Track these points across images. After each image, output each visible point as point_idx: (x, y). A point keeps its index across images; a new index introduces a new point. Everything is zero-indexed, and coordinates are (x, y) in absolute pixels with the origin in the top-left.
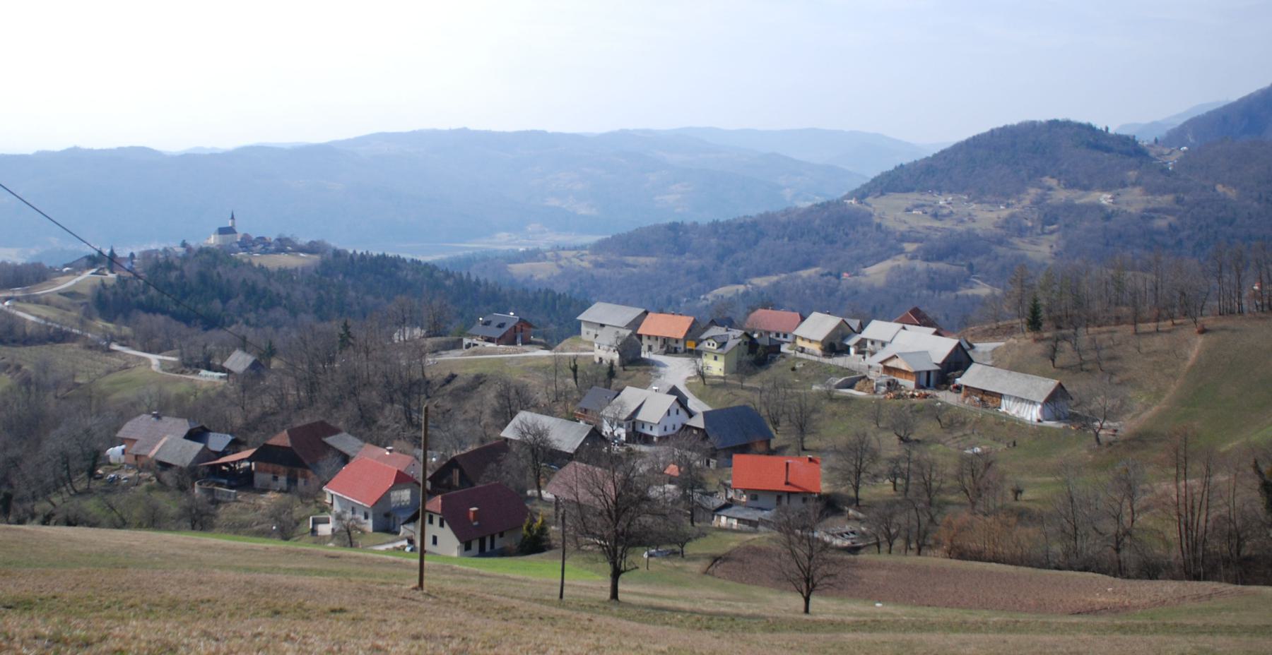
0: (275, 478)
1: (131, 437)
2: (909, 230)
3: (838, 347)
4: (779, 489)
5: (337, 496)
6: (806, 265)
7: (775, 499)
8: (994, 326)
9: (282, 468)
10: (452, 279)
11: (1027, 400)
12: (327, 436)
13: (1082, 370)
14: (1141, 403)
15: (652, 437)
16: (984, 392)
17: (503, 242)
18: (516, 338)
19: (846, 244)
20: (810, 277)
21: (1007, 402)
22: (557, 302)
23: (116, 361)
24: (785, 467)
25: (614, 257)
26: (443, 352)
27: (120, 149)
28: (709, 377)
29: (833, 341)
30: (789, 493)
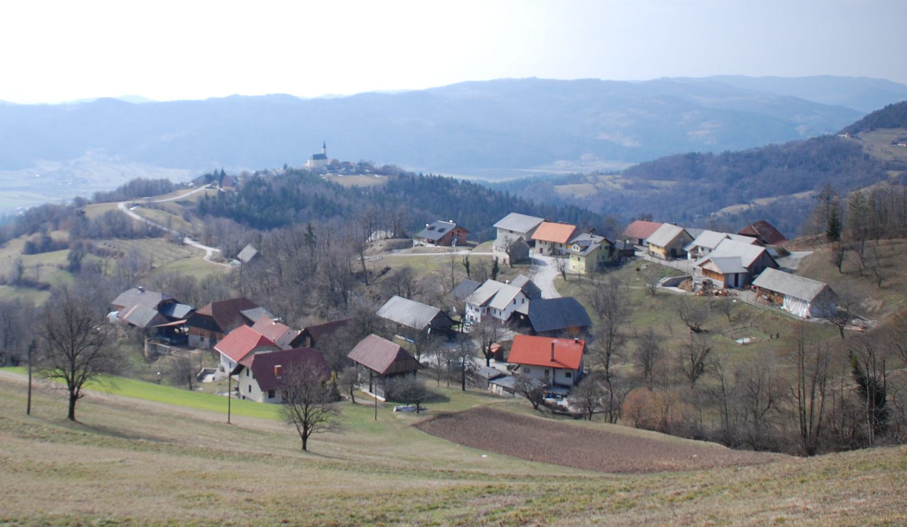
0: (202, 339)
1: (121, 305)
2: (893, 159)
3: (679, 252)
4: (545, 365)
5: (224, 356)
6: (803, 188)
7: (544, 372)
8: (814, 237)
9: (206, 332)
10: (493, 197)
11: (801, 300)
12: (245, 309)
13: (862, 275)
14: (898, 305)
15: (501, 321)
16: (772, 292)
17: (561, 168)
18: (452, 240)
19: (837, 172)
20: (804, 199)
21: (787, 300)
22: (579, 216)
23: (185, 252)
24: (551, 346)
25: (641, 181)
26: (395, 250)
27: (268, 96)
28: (569, 274)
29: (675, 247)
30: (554, 369)
